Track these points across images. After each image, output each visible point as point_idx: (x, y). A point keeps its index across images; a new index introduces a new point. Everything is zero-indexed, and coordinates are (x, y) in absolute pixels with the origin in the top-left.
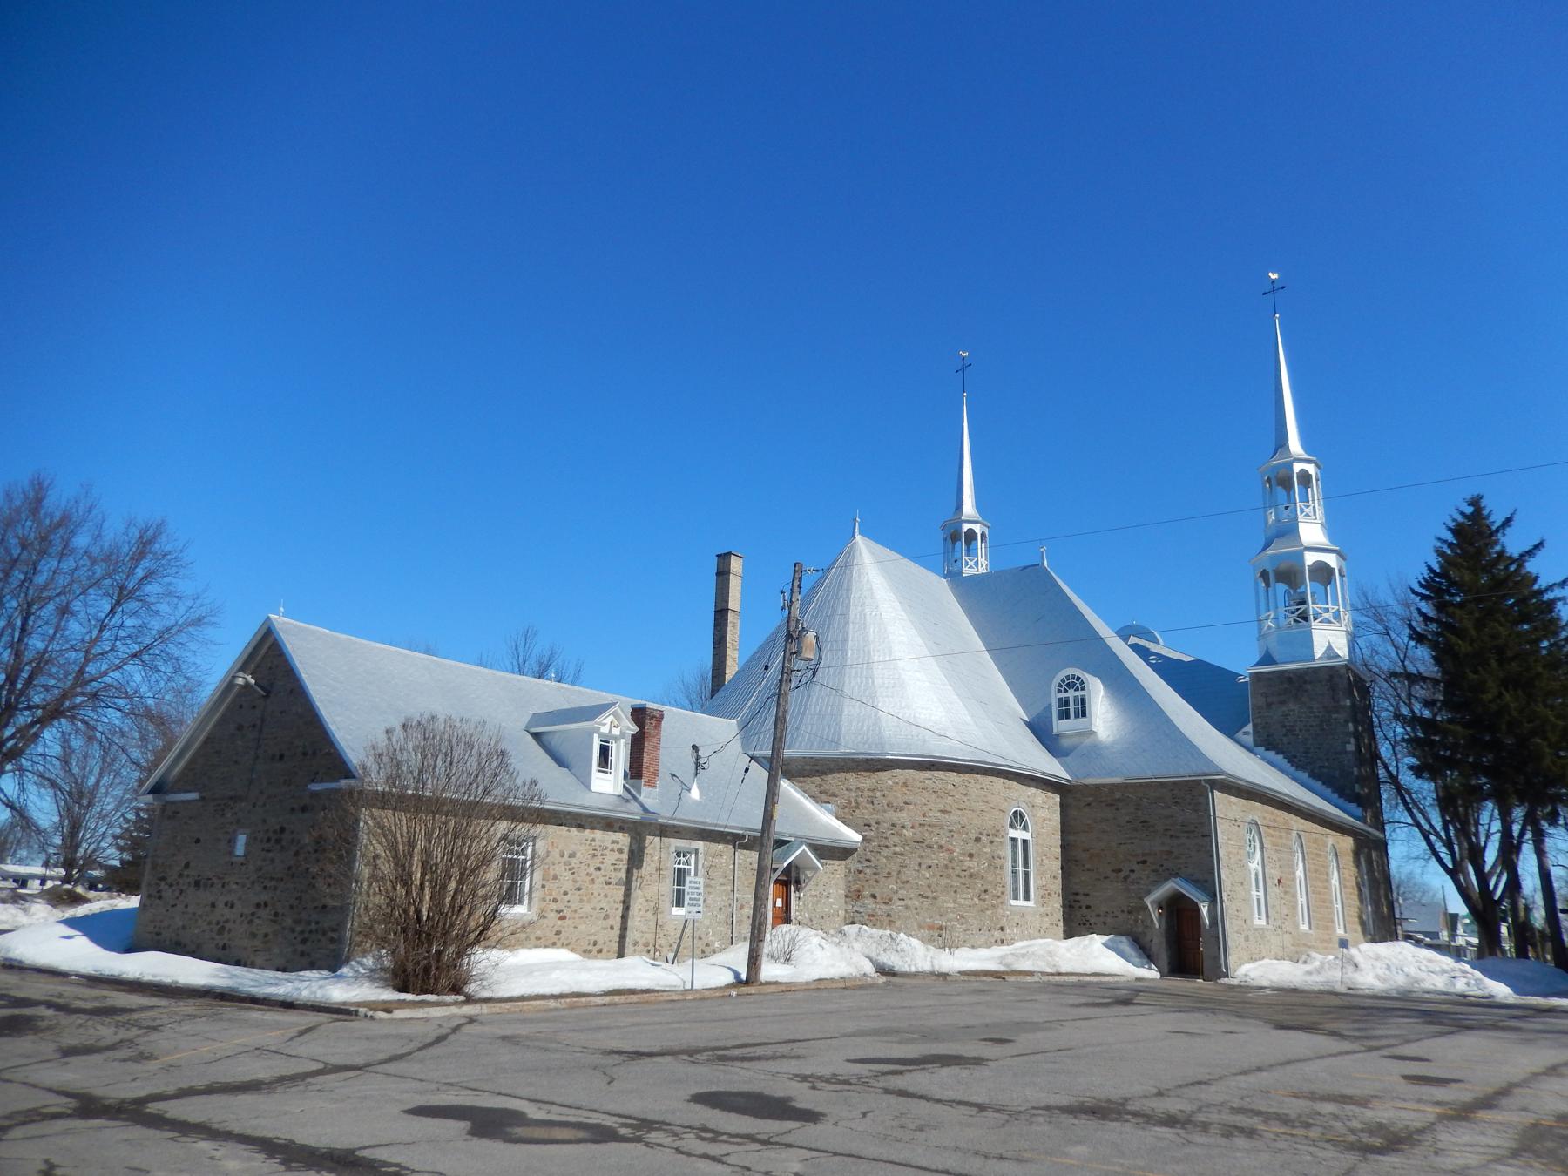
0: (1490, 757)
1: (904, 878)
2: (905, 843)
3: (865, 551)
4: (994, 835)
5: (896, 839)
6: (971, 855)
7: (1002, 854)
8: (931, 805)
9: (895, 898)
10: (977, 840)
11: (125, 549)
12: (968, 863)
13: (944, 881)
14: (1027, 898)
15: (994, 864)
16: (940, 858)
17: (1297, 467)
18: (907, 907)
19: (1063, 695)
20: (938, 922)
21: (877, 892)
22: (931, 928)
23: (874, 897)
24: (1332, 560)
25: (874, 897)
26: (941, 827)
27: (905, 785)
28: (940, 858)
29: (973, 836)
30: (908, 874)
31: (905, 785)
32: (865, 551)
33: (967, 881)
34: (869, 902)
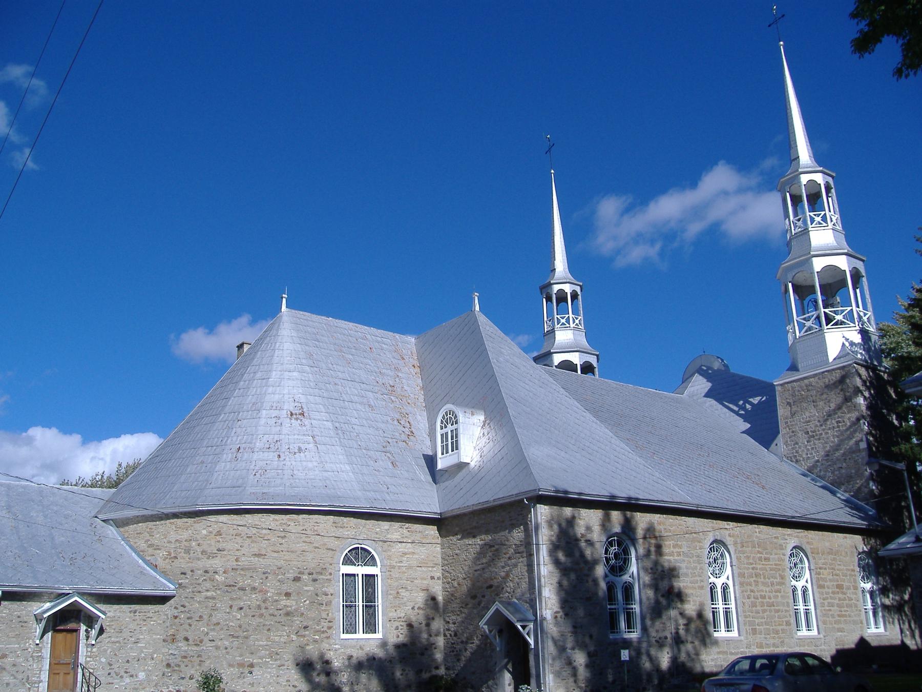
0: (833, 351)
1: (214, 620)
2: (216, 588)
3: (749, 426)
4: (318, 574)
5: (208, 585)
6: (288, 595)
7: (330, 590)
8: (243, 551)
9: (206, 639)
10: (297, 579)
11: (261, 458)
12: (284, 602)
13: (255, 622)
14: (370, 626)
15: (319, 601)
16: (254, 599)
17: (804, 179)
18: (217, 648)
19: (444, 430)
20: (249, 659)
21: (190, 635)
22: (241, 665)
23: (187, 639)
24: (842, 263)
25: (187, 639)
26: (254, 570)
27: (219, 533)
28: (254, 599)
29: (291, 576)
30: (218, 616)
31: (219, 533)
32: (749, 426)
33: (283, 619)
34: (182, 645)
